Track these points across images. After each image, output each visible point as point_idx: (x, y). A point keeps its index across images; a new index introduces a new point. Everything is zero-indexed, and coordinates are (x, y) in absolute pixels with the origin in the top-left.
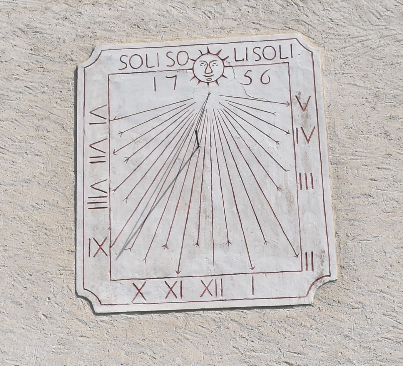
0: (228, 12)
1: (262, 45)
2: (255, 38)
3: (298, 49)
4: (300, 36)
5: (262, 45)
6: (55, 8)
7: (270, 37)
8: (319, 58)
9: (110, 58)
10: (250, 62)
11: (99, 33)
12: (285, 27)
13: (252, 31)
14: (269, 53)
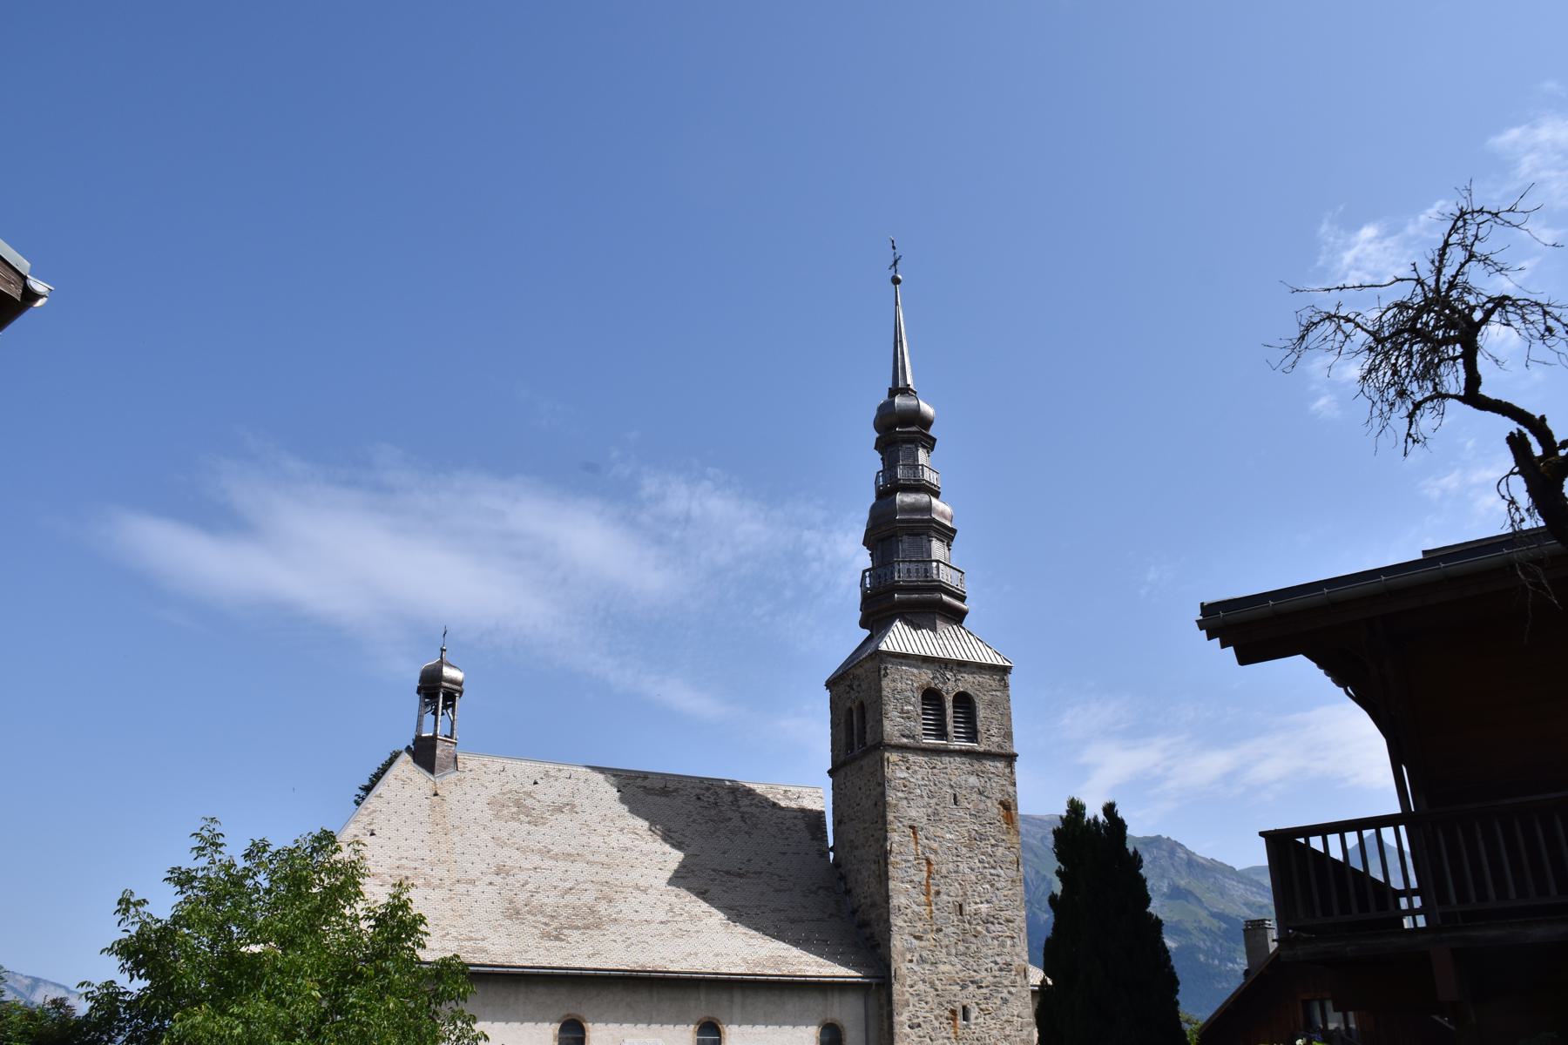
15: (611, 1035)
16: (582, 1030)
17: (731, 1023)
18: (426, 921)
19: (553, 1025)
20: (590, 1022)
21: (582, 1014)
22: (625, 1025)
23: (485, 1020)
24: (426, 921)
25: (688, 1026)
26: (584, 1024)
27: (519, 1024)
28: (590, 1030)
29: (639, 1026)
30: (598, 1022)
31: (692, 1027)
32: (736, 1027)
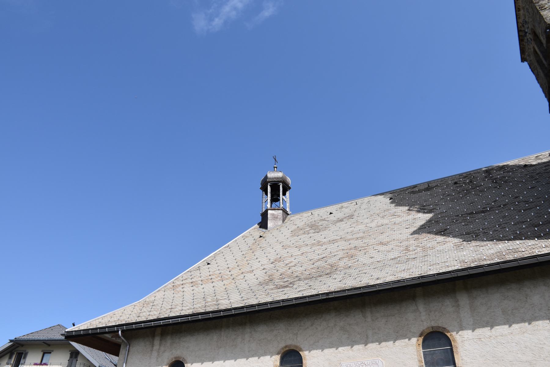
0: (366, 354)
1: (373, 361)
2: (371, 359)
3: (379, 361)
4: (380, 358)
5: (373, 361)
6: (333, 355)
7: (374, 359)
8: (384, 362)
9: (344, 365)
10: (371, 365)
11: (341, 360)
12: (542, 155)
13: (371, 358)
14: (374, 362)
17: (462, 328)
19: (274, 357)
20: (305, 351)
21: (298, 344)
22: (340, 349)
23: (219, 360)
25: (409, 339)
26: (301, 353)
28: (307, 357)
29: (356, 347)
31: (414, 340)
32: (470, 332)
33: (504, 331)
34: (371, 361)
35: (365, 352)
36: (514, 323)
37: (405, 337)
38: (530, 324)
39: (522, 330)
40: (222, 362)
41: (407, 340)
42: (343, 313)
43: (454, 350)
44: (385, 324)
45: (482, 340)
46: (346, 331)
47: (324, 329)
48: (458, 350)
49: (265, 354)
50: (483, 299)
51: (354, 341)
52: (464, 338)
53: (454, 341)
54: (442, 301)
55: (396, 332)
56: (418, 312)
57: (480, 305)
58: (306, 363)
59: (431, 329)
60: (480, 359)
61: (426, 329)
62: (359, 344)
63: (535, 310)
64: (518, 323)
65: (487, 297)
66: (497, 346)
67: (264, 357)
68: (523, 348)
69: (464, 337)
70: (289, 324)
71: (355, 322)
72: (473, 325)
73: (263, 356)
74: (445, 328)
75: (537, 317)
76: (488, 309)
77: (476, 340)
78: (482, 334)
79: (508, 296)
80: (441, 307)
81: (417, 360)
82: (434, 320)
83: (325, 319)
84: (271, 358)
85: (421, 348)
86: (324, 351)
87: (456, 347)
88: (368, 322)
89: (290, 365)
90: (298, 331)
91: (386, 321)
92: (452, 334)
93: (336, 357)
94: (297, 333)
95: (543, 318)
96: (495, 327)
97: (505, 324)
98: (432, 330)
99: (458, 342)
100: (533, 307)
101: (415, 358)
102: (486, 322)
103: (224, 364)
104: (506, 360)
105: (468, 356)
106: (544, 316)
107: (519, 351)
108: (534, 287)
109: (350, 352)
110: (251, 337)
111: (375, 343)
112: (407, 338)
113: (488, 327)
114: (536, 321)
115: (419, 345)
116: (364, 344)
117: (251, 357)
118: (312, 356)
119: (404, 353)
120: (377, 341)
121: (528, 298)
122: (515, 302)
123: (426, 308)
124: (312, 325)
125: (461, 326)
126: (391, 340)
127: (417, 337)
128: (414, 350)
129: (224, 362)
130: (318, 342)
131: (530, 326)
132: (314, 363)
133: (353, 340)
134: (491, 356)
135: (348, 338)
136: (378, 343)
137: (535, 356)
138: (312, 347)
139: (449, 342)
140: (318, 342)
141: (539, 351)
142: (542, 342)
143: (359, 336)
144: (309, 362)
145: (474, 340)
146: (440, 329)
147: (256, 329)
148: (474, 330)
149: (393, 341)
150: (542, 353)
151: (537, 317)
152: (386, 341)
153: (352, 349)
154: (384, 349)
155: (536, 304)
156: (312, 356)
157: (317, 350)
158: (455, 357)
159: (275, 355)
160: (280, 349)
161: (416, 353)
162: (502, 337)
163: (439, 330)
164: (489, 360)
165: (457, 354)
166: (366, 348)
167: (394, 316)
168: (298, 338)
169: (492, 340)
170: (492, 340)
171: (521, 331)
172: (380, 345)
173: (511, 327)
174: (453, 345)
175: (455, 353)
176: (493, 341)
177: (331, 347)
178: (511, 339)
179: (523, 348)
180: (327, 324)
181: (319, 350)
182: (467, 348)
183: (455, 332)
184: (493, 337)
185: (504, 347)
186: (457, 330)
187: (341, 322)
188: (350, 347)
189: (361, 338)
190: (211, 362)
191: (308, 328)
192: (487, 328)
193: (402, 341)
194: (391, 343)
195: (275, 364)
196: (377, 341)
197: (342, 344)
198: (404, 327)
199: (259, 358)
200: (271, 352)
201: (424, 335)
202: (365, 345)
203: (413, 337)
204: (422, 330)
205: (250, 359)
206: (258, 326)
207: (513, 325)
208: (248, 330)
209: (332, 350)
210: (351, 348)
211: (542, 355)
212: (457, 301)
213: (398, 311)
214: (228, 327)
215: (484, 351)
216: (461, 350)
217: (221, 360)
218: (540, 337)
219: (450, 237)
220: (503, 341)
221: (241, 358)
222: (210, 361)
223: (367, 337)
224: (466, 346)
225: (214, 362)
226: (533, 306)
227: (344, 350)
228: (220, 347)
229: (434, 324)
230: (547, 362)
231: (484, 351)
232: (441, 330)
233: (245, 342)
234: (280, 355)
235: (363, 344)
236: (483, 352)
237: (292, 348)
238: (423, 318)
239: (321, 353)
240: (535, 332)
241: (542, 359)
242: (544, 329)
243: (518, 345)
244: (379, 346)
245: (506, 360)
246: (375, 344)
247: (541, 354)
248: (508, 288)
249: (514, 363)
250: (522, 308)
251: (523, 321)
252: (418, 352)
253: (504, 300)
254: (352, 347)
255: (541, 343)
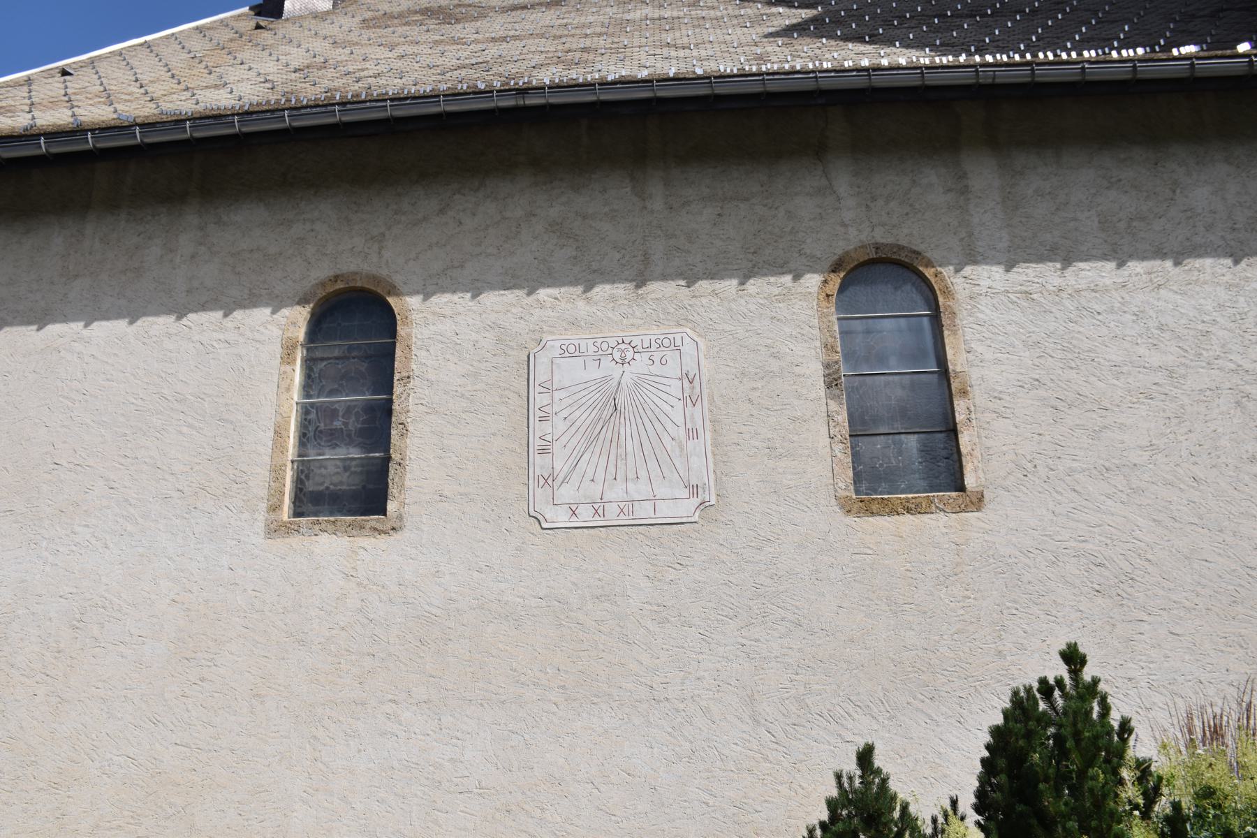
0: (637, 314)
1: (662, 337)
2: (656, 332)
3: (687, 340)
5: (662, 337)
7: (667, 331)
8: (702, 346)
9: (553, 347)
10: (653, 349)
11: (545, 328)
14: (666, 342)
15: (494, 326)
16: (387, 322)
17: (972, 257)
18: (834, 793)
19: (285, 312)
20: (411, 294)
21: (384, 272)
22: (543, 293)
23: (65, 319)
24: (834, 793)
25: (797, 278)
26: (392, 300)
27: (171, 319)
28: (415, 316)
29: (602, 291)
30: (443, 290)
31: (813, 281)
32: (997, 271)
33: (1103, 277)
34: (656, 337)
35: (635, 308)
36: (1133, 259)
37: (782, 267)
38: (1177, 263)
39: (1156, 280)
40: (77, 326)
41: (787, 279)
42: (561, 180)
43: (945, 321)
44: (715, 224)
45: (1034, 296)
46: (570, 237)
47: (488, 226)
48: (957, 321)
49: (251, 301)
50: (1044, 180)
51: (595, 271)
52: (977, 288)
53: (948, 292)
54: (912, 171)
55: (752, 250)
56: (831, 194)
57: (1032, 197)
58: (409, 335)
59: (874, 250)
60: (1025, 352)
61: (856, 249)
62: (614, 282)
63: (1194, 227)
64: (1143, 259)
65: (1056, 175)
66: (1079, 319)
67: (247, 311)
68: (1153, 330)
69: (978, 285)
70: (355, 203)
71: (606, 209)
72: (1009, 251)
73: (243, 307)
74: (918, 253)
75: (1201, 246)
76: (1058, 209)
77: (1018, 295)
78: (1036, 280)
79: (1120, 180)
80: (910, 190)
81: (818, 344)
82: (883, 225)
83: (492, 193)
84: (275, 316)
85: (833, 309)
86: (481, 296)
87: (950, 313)
88: (652, 212)
89: (944, 49)
90: (389, 228)
91: (719, 215)
92: (941, 273)
93: (525, 321)
94: (383, 235)
95: (1216, 250)
96: (1074, 264)
97: (1105, 257)
98: (876, 253)
99: (957, 296)
100: (1191, 217)
101: (811, 336)
102: (1048, 248)
103: (86, 332)
104: (1102, 361)
105: (988, 342)
106: (1219, 247)
107: (1142, 338)
108: (1197, 163)
109: (581, 304)
110: (201, 244)
111: (673, 280)
112: (790, 272)
113: (1055, 261)
114: (1195, 257)
115: (828, 296)
116: (635, 283)
117: (196, 312)
118: (434, 313)
119: (773, 318)
120: (681, 274)
121: (1178, 191)
122: (1139, 199)
123: (859, 187)
124: (442, 211)
125: (971, 250)
126: (731, 277)
127: (823, 272)
128: (810, 312)
129: (86, 326)
130: (462, 267)
131: (1177, 270)
132: (440, 338)
133: (595, 266)
134: (1059, 347)
135: (575, 258)
136: (683, 283)
137: (1186, 354)
138: (437, 284)
139: (931, 297)
140: (462, 267)
141: (1196, 341)
142: (1208, 318)
143: (618, 256)
144: (422, 334)
145: (1009, 295)
146: (904, 255)
147: (225, 218)
148: (1013, 266)
149: (739, 277)
150: (1205, 347)
151: (1201, 246)
152: (712, 276)
153: (589, 295)
154: (704, 300)
155: (1200, 211)
156: (434, 313)
157: (454, 292)
158: (947, 341)
159: (292, 305)
160: (313, 286)
161: (815, 322)
162: (1094, 294)
163: (900, 255)
164: (1052, 357)
165: (955, 333)
166: (638, 295)
167: (747, 199)
168: (383, 252)
169: (1064, 301)
170: (1064, 301)
171: (1151, 281)
172: (692, 289)
173: (1124, 268)
174: (940, 304)
175: (948, 329)
176: (1067, 303)
177: (508, 285)
178: (1120, 302)
179: (1153, 330)
180: (501, 212)
181: (461, 295)
182: (986, 318)
183: (951, 268)
184: (1070, 292)
185: (1098, 323)
186: (957, 262)
187: (552, 206)
188: (580, 289)
189: (624, 262)
190: (35, 327)
191: (425, 219)
192: (1051, 264)
193: (772, 279)
194: (729, 285)
195: (290, 335)
196: (680, 275)
197: (551, 279)
198: (781, 237)
199: (226, 315)
200: (277, 296)
201: (848, 268)
202: (638, 287)
203: (808, 272)
204: (839, 252)
205: (192, 316)
206: (233, 207)
207: (1129, 264)
208: (191, 218)
209: (511, 296)
210: (585, 292)
211: (1204, 352)
212: (963, 176)
213: (762, 186)
214: (112, 204)
215: (1038, 330)
216: (964, 322)
217: (74, 320)
218: (1202, 301)
219: (895, 46)
220: (1096, 307)
221: (157, 313)
222: (29, 323)
223: (646, 258)
224: (982, 312)
225: (45, 325)
226: (1189, 214)
227: (556, 299)
228: (76, 276)
229: (880, 236)
230: (1216, 372)
231: (1038, 330)
232: (906, 256)
233: (178, 260)
234: (311, 305)
235: (631, 281)
236: (1033, 332)
237: (359, 284)
238: (848, 216)
239: (470, 304)
240: (1189, 287)
241: (1204, 364)
242: (1216, 280)
243: (1139, 321)
244: (686, 291)
245: (1102, 361)
246: (673, 283)
247: (1204, 349)
248: (1122, 156)
249: (1125, 369)
250: (1160, 218)
251: (1160, 254)
252: (825, 320)
253: (1108, 188)
254: (588, 289)
255: (1206, 318)
